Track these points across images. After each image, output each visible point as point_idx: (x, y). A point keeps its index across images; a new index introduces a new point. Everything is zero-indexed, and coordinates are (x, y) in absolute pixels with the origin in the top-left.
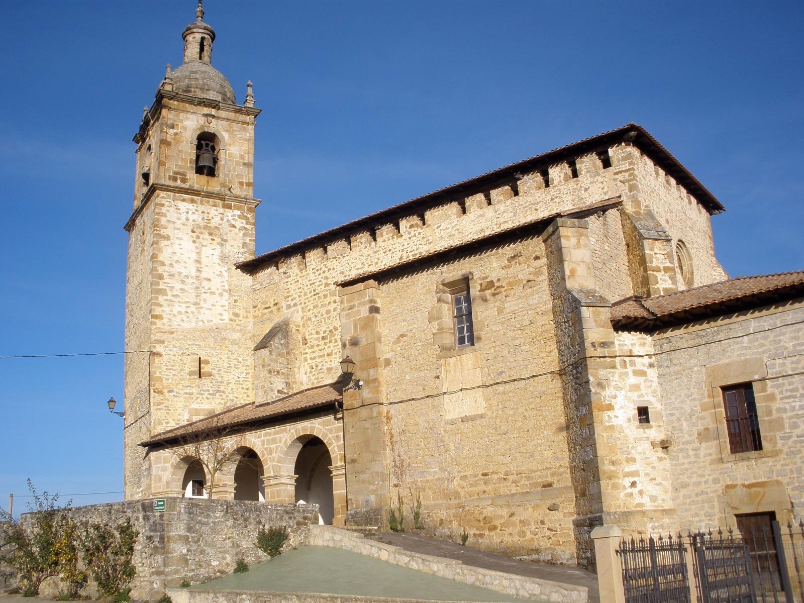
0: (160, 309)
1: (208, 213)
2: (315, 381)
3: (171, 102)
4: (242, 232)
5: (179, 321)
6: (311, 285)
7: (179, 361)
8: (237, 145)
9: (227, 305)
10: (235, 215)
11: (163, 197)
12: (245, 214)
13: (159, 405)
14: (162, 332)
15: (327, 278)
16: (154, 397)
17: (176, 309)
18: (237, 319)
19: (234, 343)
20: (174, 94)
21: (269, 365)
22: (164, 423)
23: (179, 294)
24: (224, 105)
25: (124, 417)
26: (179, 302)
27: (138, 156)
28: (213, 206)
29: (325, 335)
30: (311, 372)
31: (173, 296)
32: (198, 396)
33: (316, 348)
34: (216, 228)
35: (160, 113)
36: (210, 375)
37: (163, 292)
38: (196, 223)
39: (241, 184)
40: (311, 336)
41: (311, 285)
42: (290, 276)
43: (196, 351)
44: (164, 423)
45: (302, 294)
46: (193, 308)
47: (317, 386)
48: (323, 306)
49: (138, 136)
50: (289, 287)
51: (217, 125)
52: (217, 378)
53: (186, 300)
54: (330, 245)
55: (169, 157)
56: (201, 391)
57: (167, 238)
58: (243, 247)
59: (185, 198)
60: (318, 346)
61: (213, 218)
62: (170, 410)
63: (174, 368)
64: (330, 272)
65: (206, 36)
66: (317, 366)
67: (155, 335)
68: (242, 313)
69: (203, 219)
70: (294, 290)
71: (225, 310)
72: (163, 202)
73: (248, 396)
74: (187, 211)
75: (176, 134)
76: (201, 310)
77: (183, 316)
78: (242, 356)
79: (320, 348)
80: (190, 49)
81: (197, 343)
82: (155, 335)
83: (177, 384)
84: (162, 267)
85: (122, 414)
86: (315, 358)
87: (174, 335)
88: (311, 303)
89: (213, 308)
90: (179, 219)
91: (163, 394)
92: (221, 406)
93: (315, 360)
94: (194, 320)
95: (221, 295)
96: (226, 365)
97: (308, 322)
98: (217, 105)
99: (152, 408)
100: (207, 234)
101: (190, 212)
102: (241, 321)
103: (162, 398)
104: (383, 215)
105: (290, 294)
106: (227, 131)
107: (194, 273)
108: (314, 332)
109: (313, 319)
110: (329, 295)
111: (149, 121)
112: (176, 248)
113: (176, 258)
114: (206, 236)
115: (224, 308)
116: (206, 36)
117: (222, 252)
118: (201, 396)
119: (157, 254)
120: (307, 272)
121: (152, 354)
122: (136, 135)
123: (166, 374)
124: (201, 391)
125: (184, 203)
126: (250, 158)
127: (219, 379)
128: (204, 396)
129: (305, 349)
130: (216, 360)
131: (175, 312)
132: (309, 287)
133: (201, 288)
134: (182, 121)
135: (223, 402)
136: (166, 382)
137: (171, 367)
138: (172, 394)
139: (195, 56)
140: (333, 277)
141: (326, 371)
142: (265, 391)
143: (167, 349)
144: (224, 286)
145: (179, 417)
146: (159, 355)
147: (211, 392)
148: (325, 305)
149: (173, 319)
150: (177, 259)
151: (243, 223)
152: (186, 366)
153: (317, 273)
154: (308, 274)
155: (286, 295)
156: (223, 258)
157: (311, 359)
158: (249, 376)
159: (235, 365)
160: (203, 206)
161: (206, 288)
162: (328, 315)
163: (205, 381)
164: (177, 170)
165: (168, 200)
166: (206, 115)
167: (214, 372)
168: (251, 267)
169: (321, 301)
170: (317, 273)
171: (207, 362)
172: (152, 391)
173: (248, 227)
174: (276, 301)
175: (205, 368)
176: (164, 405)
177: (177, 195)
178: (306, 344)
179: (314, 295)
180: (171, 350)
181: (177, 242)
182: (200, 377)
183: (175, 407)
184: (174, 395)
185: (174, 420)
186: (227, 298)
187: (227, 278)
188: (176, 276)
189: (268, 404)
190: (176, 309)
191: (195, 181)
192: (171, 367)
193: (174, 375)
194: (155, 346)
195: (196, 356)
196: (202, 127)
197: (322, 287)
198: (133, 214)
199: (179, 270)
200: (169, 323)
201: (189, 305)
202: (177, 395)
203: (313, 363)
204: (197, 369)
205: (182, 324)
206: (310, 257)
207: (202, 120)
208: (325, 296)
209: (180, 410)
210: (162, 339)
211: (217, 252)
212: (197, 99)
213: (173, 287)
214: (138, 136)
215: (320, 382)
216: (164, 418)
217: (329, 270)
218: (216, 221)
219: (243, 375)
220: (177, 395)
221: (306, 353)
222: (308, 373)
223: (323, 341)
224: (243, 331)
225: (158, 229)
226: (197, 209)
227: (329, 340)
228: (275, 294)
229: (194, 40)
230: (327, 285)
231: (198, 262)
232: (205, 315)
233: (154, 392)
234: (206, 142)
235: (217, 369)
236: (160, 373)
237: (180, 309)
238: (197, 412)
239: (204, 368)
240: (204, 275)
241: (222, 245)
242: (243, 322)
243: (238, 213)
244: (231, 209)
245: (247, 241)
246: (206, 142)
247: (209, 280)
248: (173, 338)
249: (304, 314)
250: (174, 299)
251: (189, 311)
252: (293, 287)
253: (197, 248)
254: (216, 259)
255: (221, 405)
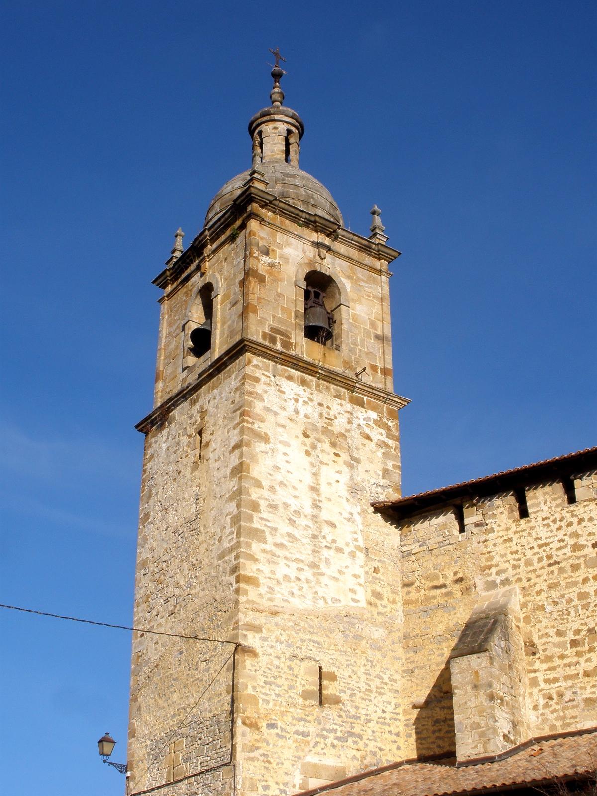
0: (254, 567)
1: (328, 408)
2: (558, 724)
3: (264, 211)
4: (382, 450)
5: (286, 594)
6: (540, 546)
7: (286, 669)
8: (365, 304)
9: (363, 576)
10: (368, 419)
11: (256, 366)
12: (385, 420)
13: (251, 751)
14: (257, 611)
15: (576, 535)
16: (244, 735)
17: (281, 570)
18: (378, 602)
19: (376, 647)
20: (271, 198)
21: (490, 685)
22: (260, 788)
23: (285, 543)
24: (344, 233)
25: (129, 774)
26: (286, 558)
27: (165, 307)
28: (335, 397)
29: (577, 637)
30: (547, 706)
31: (276, 545)
32: (318, 740)
33: (557, 662)
34: (342, 435)
35: (243, 227)
36: (337, 701)
37: (257, 534)
38: (310, 421)
39: (374, 368)
40: (544, 640)
41: (540, 546)
42: (492, 530)
43: (315, 653)
44: (260, 788)
45: (522, 563)
46: (308, 573)
47: (561, 731)
48: (568, 585)
49: (168, 273)
50: (489, 549)
51: (333, 264)
52: (349, 708)
53: (298, 556)
54: (580, 478)
55: (263, 301)
56: (323, 730)
57: (265, 439)
58: (383, 477)
59: (291, 374)
60: (562, 657)
61: (336, 418)
62: (270, 763)
63: (279, 681)
64: (583, 524)
65: (294, 129)
66: (561, 695)
67: (246, 614)
68: (386, 593)
69: (321, 416)
70: (502, 556)
71: (360, 585)
72: (257, 375)
73: (398, 748)
74: (295, 397)
75: (272, 265)
76: (321, 578)
77: (293, 584)
78: (387, 672)
79: (566, 661)
80: (269, 145)
81: (315, 638)
82: (246, 614)
83: (283, 714)
84: (257, 489)
85: (124, 769)
86: (556, 680)
87: (277, 619)
88: (542, 578)
89: (341, 577)
90: (283, 409)
91: (258, 729)
92: (357, 763)
93: (557, 684)
94: (310, 596)
95: (352, 555)
96: (364, 686)
97: (538, 613)
98: (335, 231)
99: (240, 756)
100: (328, 444)
101: (301, 400)
102: (385, 607)
103: (256, 737)
104: (416, 503)
105: (494, 562)
106: (349, 277)
107: (308, 510)
108: (552, 632)
109: (549, 608)
110: (582, 566)
111: (204, 246)
112: (280, 460)
113: (278, 477)
114: (326, 446)
115: (358, 580)
116: (294, 129)
117: (352, 479)
118: (322, 741)
119: (249, 465)
120: (531, 525)
121: (238, 648)
122: (164, 272)
123: (263, 690)
124: (323, 730)
125: (291, 383)
126: (386, 330)
127: (353, 712)
128: (329, 741)
129: (531, 663)
130: (346, 674)
131: (279, 576)
132: (536, 549)
133: (320, 538)
134: (280, 246)
135: (358, 754)
136: (265, 706)
137: (272, 679)
138: (274, 731)
139: (278, 157)
140: (589, 534)
141: (582, 705)
142: (482, 735)
143: (266, 643)
144: (356, 540)
145: (287, 778)
146: (251, 652)
147: (339, 734)
148: (575, 583)
149: (276, 588)
150: (282, 479)
151: (382, 435)
152: (299, 681)
153: (554, 527)
154: (532, 528)
155: (483, 563)
156: (355, 490)
157: (547, 681)
158: (400, 710)
159: (377, 687)
160: (321, 394)
161: (329, 538)
162: (584, 602)
163: (330, 713)
164: (275, 325)
165: (266, 373)
166: (318, 245)
167: (344, 697)
168: (401, 513)
169: (565, 575)
170: (554, 527)
171: (333, 677)
172: (239, 722)
173: (390, 442)
174: (460, 575)
175: (331, 689)
176: (261, 751)
177: (279, 366)
178: (534, 654)
179: (550, 565)
180: (272, 647)
181: (281, 448)
182: (321, 704)
183: (279, 757)
184: (277, 734)
185: (277, 783)
186: (362, 563)
187: (361, 527)
188: (281, 509)
189: (491, 760)
190: (281, 570)
191: (304, 348)
192: (272, 679)
193: (278, 695)
194: (245, 636)
195: (314, 663)
196: (311, 263)
197: (567, 551)
198: (170, 399)
199: (285, 500)
200: (270, 596)
201: (301, 565)
202: (283, 734)
203: (553, 689)
204: (317, 688)
205: (291, 599)
206: (536, 498)
207: (311, 252)
208: (575, 568)
209: (287, 765)
210: (257, 623)
211: (345, 478)
212: (304, 215)
213: (276, 530)
214: (168, 273)
215: (568, 725)
216: (260, 777)
217: (581, 521)
218: (340, 425)
219: (390, 708)
220: (283, 734)
221: (535, 671)
222: (541, 707)
223: (574, 650)
224: (388, 626)
225: (250, 420)
226: (311, 396)
227: (586, 647)
228: (456, 562)
229: (276, 131)
230: (576, 547)
231: (315, 489)
232: (330, 590)
233: (244, 723)
234: (318, 285)
235: (349, 692)
236: (254, 688)
237: (287, 571)
238: (313, 770)
239: (327, 687)
240: (324, 515)
241: (351, 467)
242: (388, 610)
243: (374, 415)
244: (363, 407)
245: (390, 467)
246: (318, 285)
247: (333, 525)
248: (277, 625)
249: (528, 599)
250: (278, 551)
251: (303, 577)
252: (500, 549)
253: (312, 465)
254: (342, 489)
255: (355, 761)
